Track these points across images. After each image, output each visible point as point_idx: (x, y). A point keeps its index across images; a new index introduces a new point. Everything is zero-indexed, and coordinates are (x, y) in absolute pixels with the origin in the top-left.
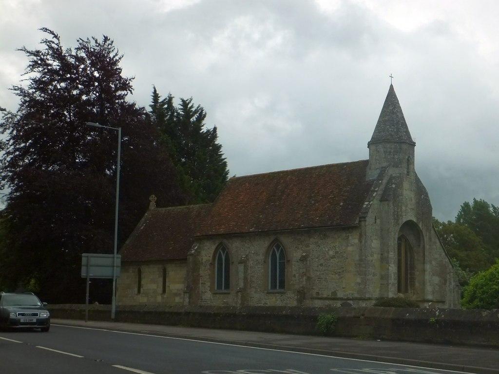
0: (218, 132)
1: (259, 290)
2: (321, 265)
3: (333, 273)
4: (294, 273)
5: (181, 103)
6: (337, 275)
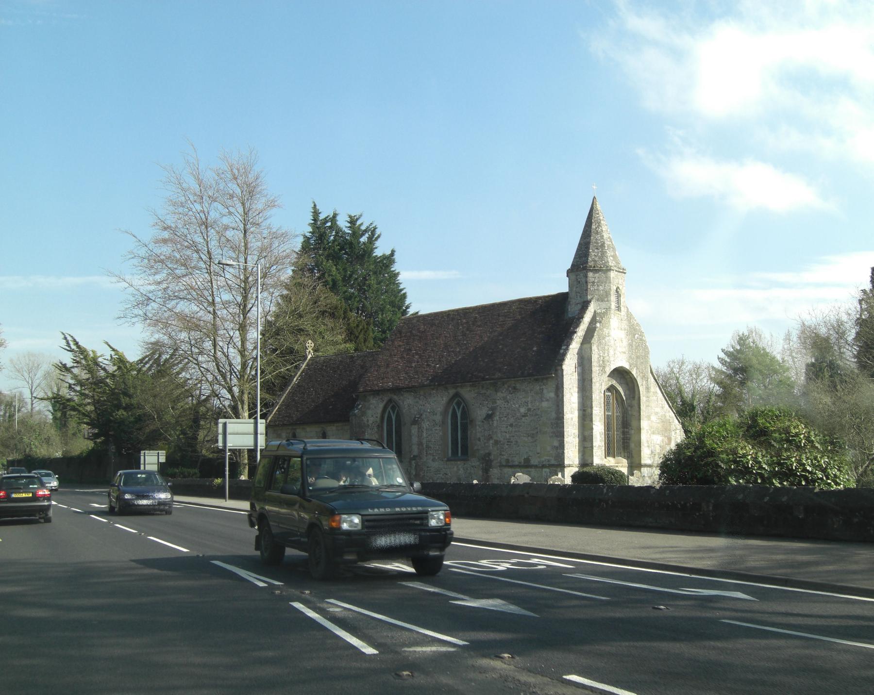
0: (396, 257)
1: (437, 458)
2: (511, 425)
3: (525, 435)
4: (479, 435)
5: (349, 219)
6: (530, 438)
